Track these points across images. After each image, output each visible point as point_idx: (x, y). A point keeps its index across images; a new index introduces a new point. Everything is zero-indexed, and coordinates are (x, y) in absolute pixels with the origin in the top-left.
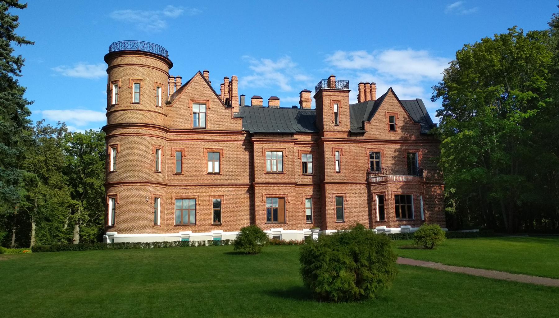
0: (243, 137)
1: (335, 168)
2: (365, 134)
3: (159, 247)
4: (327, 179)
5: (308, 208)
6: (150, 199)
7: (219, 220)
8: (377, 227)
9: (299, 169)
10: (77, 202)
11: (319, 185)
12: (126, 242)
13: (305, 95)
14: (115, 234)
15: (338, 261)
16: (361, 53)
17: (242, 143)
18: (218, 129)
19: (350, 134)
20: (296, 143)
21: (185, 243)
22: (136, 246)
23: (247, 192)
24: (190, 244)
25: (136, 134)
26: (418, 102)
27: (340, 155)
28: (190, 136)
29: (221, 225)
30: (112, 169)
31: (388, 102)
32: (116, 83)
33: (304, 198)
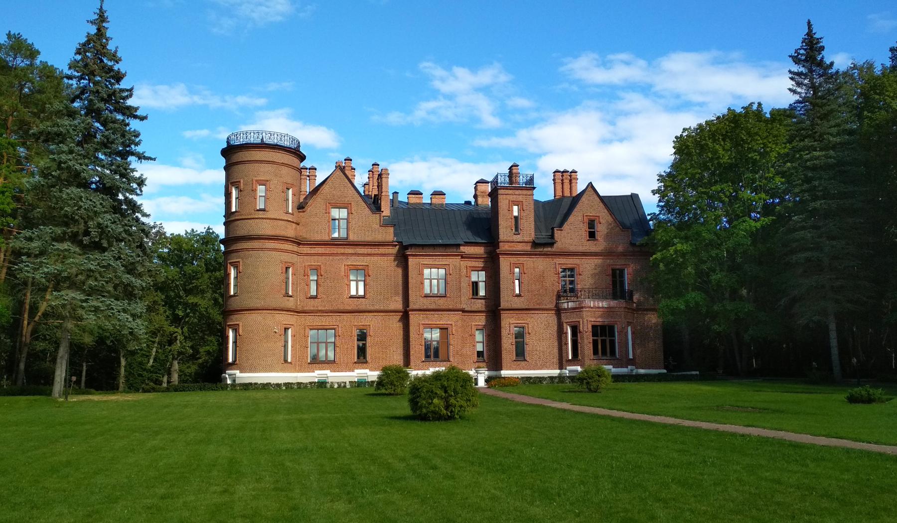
0: (395, 250)
1: (514, 290)
2: (555, 245)
3: (292, 388)
4: (504, 304)
5: (479, 341)
6: (278, 329)
7: (365, 357)
8: (568, 368)
9: (467, 291)
10: (176, 330)
11: (494, 312)
12: (253, 382)
13: (481, 187)
14: (237, 373)
15: (432, 392)
16: (623, 56)
17: (393, 258)
18: (363, 239)
19: (535, 244)
20: (463, 257)
21: (322, 384)
22: (266, 386)
23: (399, 321)
24: (328, 385)
25: (262, 249)
26: (634, 198)
27: (520, 273)
28: (328, 250)
29: (366, 362)
30: (232, 293)
31: (586, 202)
32: (236, 184)
33: (474, 328)
